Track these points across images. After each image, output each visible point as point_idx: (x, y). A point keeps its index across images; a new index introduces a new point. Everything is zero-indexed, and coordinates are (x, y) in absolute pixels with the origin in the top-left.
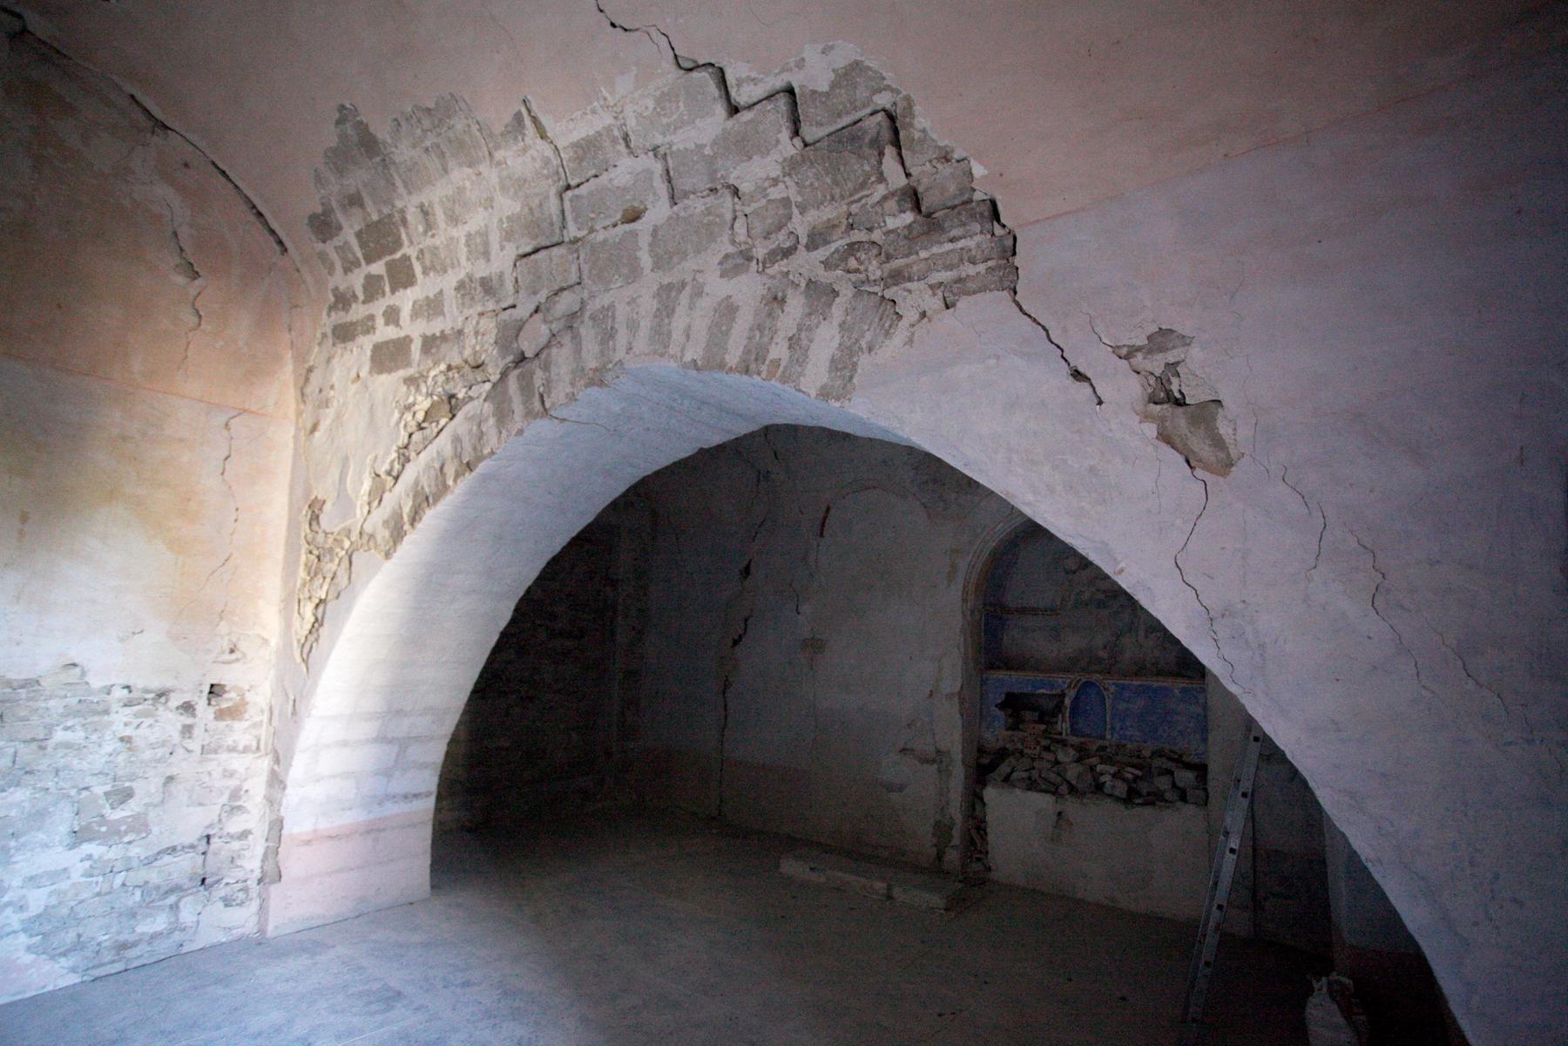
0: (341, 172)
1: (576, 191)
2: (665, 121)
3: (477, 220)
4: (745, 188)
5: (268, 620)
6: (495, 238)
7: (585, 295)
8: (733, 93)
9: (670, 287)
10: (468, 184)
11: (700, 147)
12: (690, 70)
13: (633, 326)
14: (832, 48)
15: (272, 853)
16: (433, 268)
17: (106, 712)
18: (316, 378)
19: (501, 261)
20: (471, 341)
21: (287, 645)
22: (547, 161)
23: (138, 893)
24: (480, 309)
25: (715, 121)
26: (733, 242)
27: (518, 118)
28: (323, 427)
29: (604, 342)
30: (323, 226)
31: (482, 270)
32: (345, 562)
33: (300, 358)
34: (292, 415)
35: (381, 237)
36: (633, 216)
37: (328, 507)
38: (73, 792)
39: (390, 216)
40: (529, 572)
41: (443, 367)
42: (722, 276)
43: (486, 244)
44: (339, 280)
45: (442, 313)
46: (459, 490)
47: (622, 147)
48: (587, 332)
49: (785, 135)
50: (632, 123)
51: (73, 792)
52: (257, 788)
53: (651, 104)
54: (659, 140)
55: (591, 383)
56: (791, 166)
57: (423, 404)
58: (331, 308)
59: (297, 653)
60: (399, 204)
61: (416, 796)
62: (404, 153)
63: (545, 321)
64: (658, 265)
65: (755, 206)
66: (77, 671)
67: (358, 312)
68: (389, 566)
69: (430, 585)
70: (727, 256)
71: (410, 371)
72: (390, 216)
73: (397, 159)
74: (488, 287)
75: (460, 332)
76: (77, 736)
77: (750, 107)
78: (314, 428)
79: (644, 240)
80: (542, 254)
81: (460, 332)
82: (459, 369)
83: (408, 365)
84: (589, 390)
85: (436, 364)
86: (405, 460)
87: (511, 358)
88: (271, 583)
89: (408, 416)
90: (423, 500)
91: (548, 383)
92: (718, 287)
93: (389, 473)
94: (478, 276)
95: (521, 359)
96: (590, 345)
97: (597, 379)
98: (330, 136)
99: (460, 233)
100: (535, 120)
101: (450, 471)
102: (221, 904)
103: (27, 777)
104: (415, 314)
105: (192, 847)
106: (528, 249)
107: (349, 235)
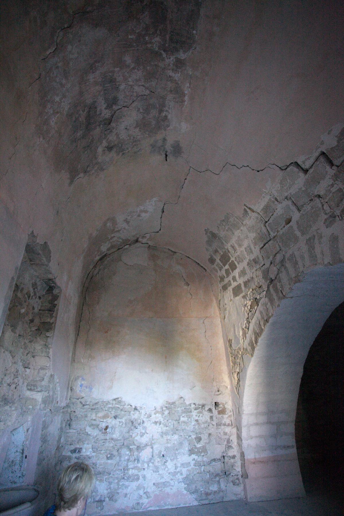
0: (210, 246)
1: (269, 222)
2: (285, 188)
3: (246, 243)
4: (322, 193)
5: (226, 381)
6: (252, 247)
7: (284, 253)
8: (303, 167)
9: (310, 239)
10: (240, 234)
11: (300, 189)
12: (286, 169)
13: (302, 257)
14: (331, 130)
15: (243, 466)
16: (240, 261)
17: (191, 412)
18: (221, 302)
19: (256, 252)
20: (256, 279)
21: (232, 388)
22: (257, 218)
23: (208, 474)
24: (255, 269)
25: (302, 178)
26: (326, 214)
27: (245, 209)
28: (226, 317)
29: (295, 267)
30: (212, 261)
31: (252, 257)
32: (241, 359)
33: (217, 299)
34: (218, 314)
35: (225, 258)
36: (289, 221)
37: (233, 341)
38: (187, 437)
39: (225, 252)
40: (305, 354)
41: (251, 290)
42: (327, 227)
43: (251, 249)
44: (219, 274)
45: (246, 274)
46: (266, 329)
47: (276, 203)
48: (288, 265)
49: (328, 168)
50: (276, 194)
51: (187, 437)
52: (234, 438)
53: (279, 185)
54: (286, 194)
55: (296, 282)
56: (336, 177)
57: (249, 303)
58: (220, 282)
59: (235, 390)
60: (226, 247)
61: (288, 447)
62: (222, 234)
63: (275, 266)
64: (303, 234)
65: (328, 198)
66: (182, 399)
67: (226, 280)
68: (253, 359)
69: (269, 365)
70: (326, 220)
71: (243, 294)
72: (225, 252)
73: (221, 236)
74: (255, 261)
75: (252, 278)
76: (185, 419)
77: (311, 167)
78: (224, 318)
79: (295, 227)
80: (267, 245)
81: (252, 278)
82: (255, 289)
83: (242, 292)
84: (297, 285)
85: (249, 290)
86: (249, 322)
87: (268, 281)
88: (225, 368)
89: (246, 308)
90: (257, 335)
91: (282, 287)
92: (327, 232)
93: (246, 327)
94: (252, 259)
95: (272, 281)
96: (291, 270)
97: (297, 280)
98: (205, 238)
99: (243, 249)
100: (250, 208)
101: (262, 323)
102: (232, 484)
103: (177, 432)
104: (240, 276)
105: (220, 460)
106: (262, 245)
107: (218, 261)
